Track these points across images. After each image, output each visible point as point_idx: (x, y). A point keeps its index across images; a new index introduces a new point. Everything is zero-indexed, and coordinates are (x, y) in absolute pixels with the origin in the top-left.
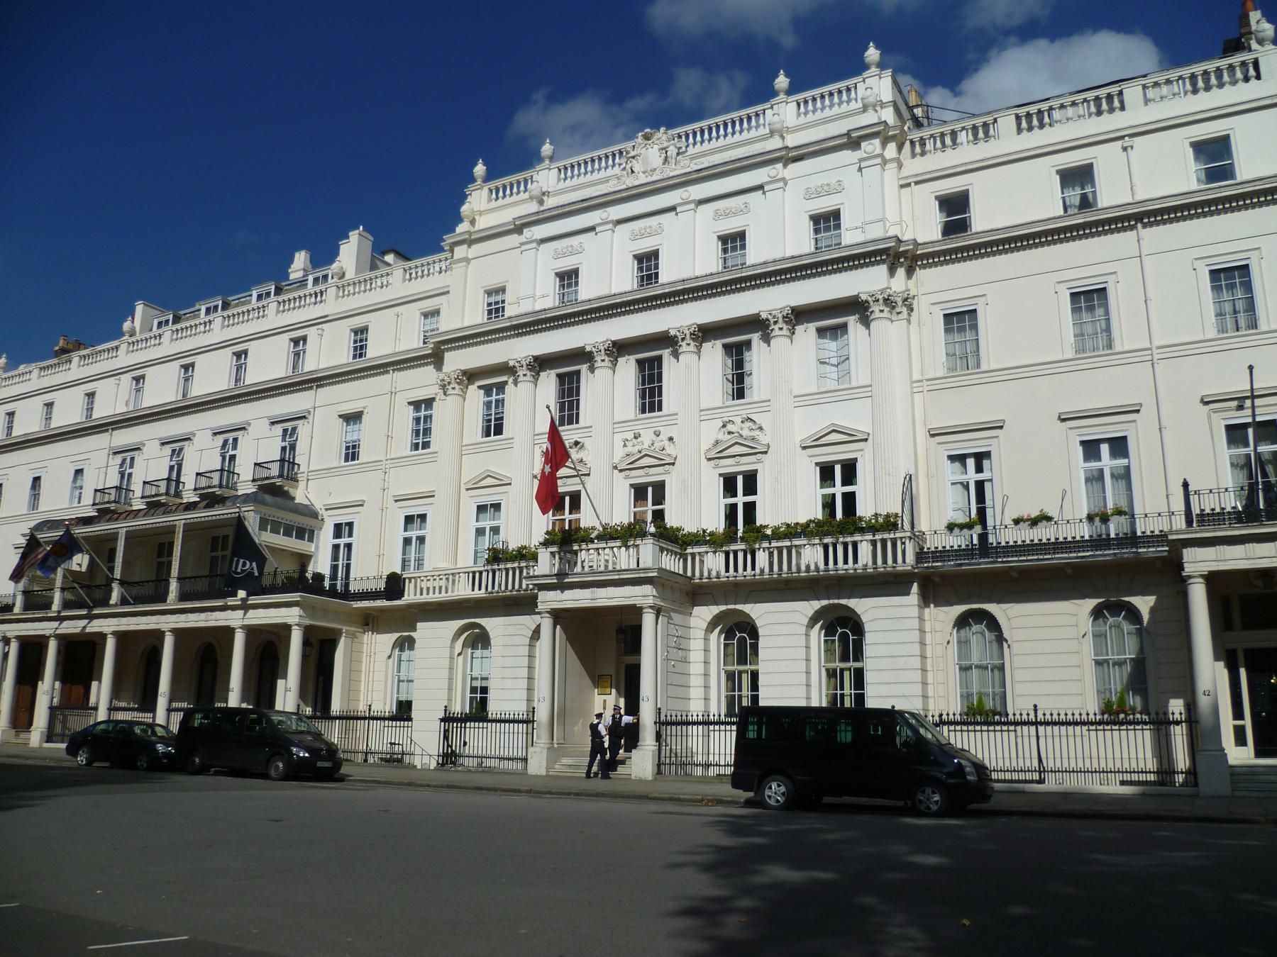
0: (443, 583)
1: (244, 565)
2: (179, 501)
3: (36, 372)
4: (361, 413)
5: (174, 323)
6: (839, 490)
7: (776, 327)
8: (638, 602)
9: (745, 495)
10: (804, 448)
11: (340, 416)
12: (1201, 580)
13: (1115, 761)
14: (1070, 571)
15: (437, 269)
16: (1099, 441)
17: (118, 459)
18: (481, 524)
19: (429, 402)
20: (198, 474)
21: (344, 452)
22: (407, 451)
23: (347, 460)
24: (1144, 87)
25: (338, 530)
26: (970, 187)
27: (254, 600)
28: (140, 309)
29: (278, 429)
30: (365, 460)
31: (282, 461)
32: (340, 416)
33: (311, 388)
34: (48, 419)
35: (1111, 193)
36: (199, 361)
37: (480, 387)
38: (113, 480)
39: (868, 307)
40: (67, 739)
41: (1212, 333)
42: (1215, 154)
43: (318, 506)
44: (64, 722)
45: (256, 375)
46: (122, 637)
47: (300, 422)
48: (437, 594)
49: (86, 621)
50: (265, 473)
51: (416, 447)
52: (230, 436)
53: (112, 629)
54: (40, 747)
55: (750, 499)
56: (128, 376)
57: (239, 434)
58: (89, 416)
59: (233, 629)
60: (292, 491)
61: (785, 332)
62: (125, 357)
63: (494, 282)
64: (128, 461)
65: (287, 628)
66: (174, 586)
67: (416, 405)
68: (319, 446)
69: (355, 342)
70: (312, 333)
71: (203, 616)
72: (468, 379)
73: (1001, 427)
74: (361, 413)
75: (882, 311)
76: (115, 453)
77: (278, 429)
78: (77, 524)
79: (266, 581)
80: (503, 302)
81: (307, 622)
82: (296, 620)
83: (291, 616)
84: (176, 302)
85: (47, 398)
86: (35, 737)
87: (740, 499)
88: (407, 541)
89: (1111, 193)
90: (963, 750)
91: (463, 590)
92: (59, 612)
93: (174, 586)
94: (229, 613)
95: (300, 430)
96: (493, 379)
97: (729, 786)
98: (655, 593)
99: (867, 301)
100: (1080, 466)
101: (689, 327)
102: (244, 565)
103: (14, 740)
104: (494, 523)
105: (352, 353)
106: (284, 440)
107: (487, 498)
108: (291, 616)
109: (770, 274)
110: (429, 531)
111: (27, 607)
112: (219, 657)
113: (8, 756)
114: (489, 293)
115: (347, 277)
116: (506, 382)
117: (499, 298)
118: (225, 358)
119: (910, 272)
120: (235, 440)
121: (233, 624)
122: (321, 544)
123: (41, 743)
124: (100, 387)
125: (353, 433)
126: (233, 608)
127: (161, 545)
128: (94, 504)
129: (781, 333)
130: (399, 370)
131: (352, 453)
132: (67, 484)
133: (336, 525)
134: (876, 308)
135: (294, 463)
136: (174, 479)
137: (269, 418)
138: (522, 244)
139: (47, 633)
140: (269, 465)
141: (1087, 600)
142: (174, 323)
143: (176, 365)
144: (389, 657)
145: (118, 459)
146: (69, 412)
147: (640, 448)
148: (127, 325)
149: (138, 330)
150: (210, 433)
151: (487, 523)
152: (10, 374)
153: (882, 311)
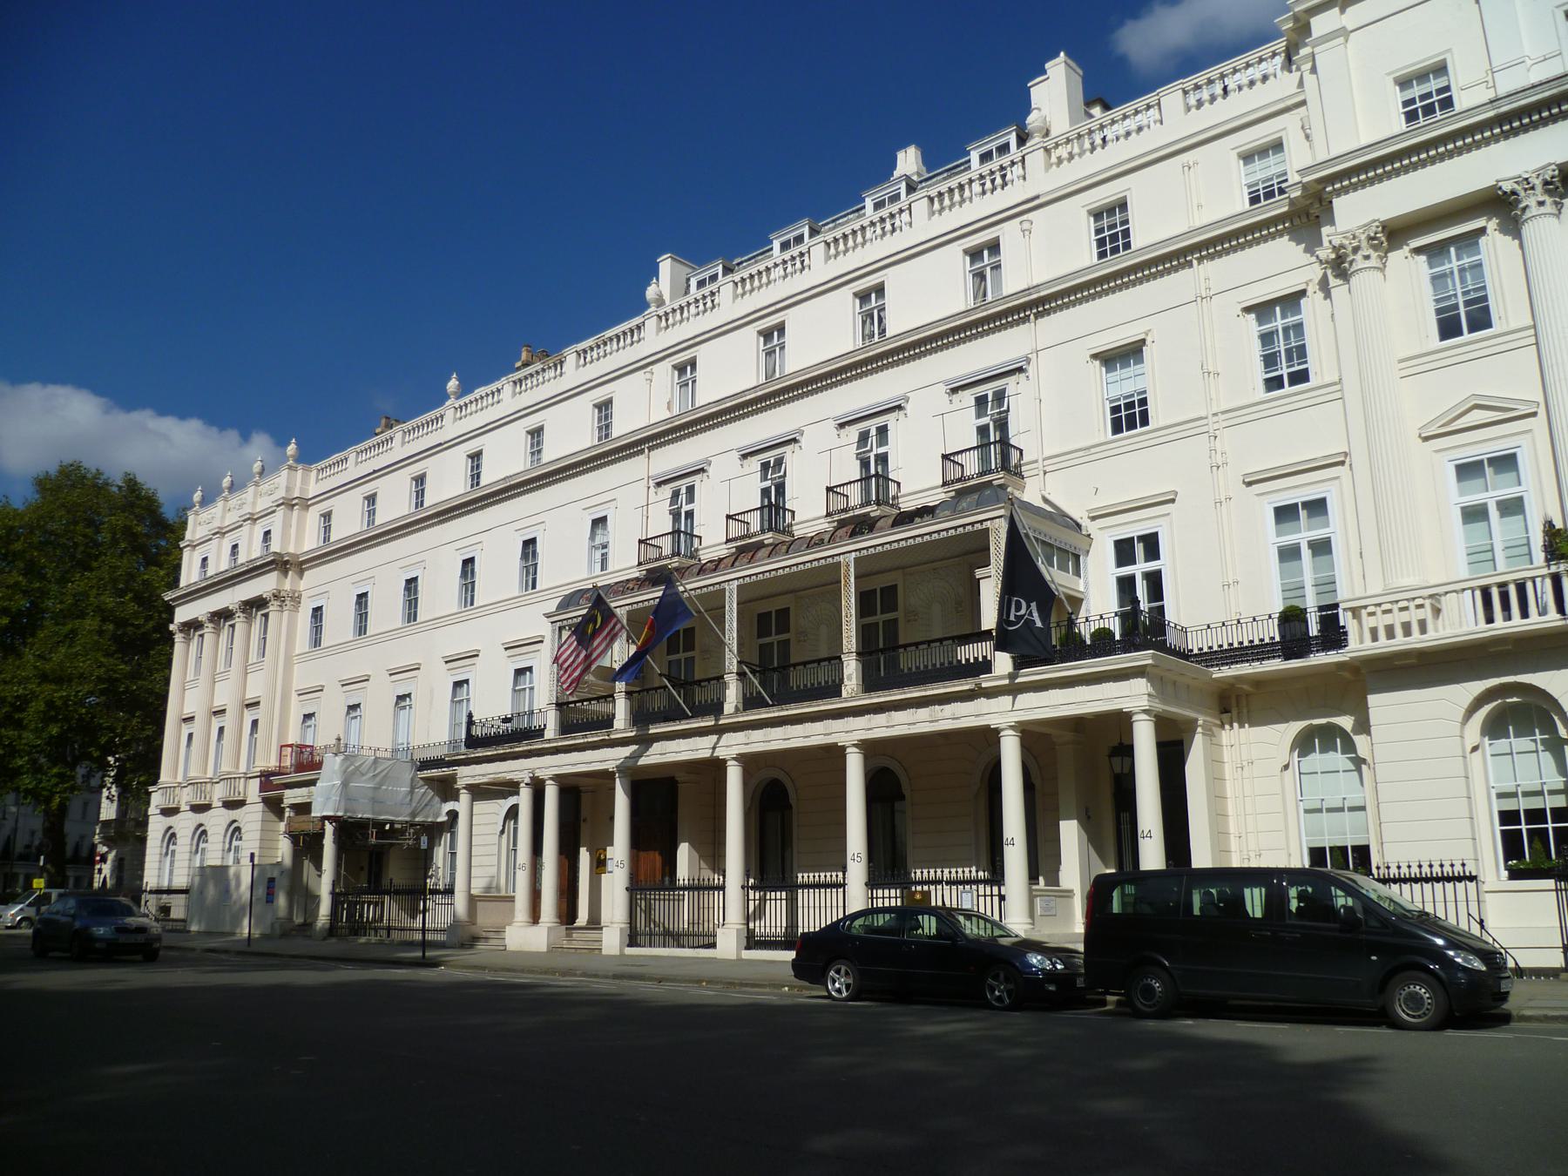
0: (1426, 613)
2: (693, 562)
3: (508, 389)
4: (1143, 341)
7: (1359, 257)
8: (1126, 705)
10: (1426, 439)
11: (1095, 356)
12: (1011, 732)
13: (527, 937)
14: (1346, 675)
15: (1087, 145)
17: (667, 491)
18: (1289, 539)
19: (1292, 301)
20: (729, 517)
21: (1109, 417)
22: (1260, 393)
23: (1117, 428)
24: (1185, 92)
25: (1124, 552)
26: (1282, 134)
27: (1029, 675)
28: (666, 265)
29: (755, 464)
30: (1162, 424)
31: (676, 532)
32: (1095, 356)
33: (642, 452)
34: (372, 513)
35: (1150, 230)
36: (702, 353)
37: (1418, 251)
38: (662, 523)
39: (1518, 201)
41: (1110, 437)
42: (1112, 228)
43: (1077, 512)
44: (648, 911)
45: (799, 357)
46: (1034, 737)
47: (788, 449)
48: (1368, 643)
49: (715, 737)
50: (653, 553)
51: (1274, 384)
52: (683, 485)
53: (735, 751)
54: (622, 955)
56: (667, 365)
57: (889, 419)
59: (997, 732)
61: (1374, 262)
62: (653, 338)
63: (1417, 56)
64: (683, 491)
65: (1120, 722)
66: (851, 668)
67: (1262, 310)
68: (1056, 411)
69: (1099, 231)
71: (923, 713)
72: (1388, 239)
73: (1173, 501)
74: (1143, 341)
75: (1541, 204)
76: (659, 484)
77: (755, 464)
78: (616, 593)
80: (1447, 88)
81: (1159, 707)
82: (1144, 703)
83: (1133, 696)
84: (728, 235)
85: (532, 422)
86: (611, 940)
88: (1289, 554)
89: (1150, 230)
90: (1423, 913)
91: (1462, 622)
92: (1012, 676)
94: (982, 704)
95: (788, 459)
98: (1150, 689)
99: (1514, 193)
100: (1271, 537)
101: (1538, 172)
103: (565, 944)
104: (1318, 534)
105: (1095, 251)
106: (764, 478)
107: (1297, 492)
108: (1133, 696)
110: (1336, 527)
111: (566, 728)
112: (793, 801)
113: (565, 973)
114: (1404, 83)
115: (1053, 133)
116: (1482, 231)
117: (1434, 84)
118: (843, 304)
119: (301, 573)
120: (691, 490)
121: (993, 721)
122: (1090, 579)
123: (621, 950)
124: (618, 391)
125: (1125, 383)
126: (991, 693)
129: (1367, 264)
130: (1211, 257)
131: (1129, 416)
132: (603, 532)
134: (1530, 201)
135: (692, 536)
136: (774, 506)
137: (946, 383)
139: (610, 766)
140: (845, 490)
141: (1285, 719)
143: (750, 332)
144: (502, 832)
145: (667, 491)
146: (570, 432)
148: (651, 292)
149: (666, 297)
150: (736, 455)
151: (1304, 533)
152: (466, 399)
153: (1541, 204)
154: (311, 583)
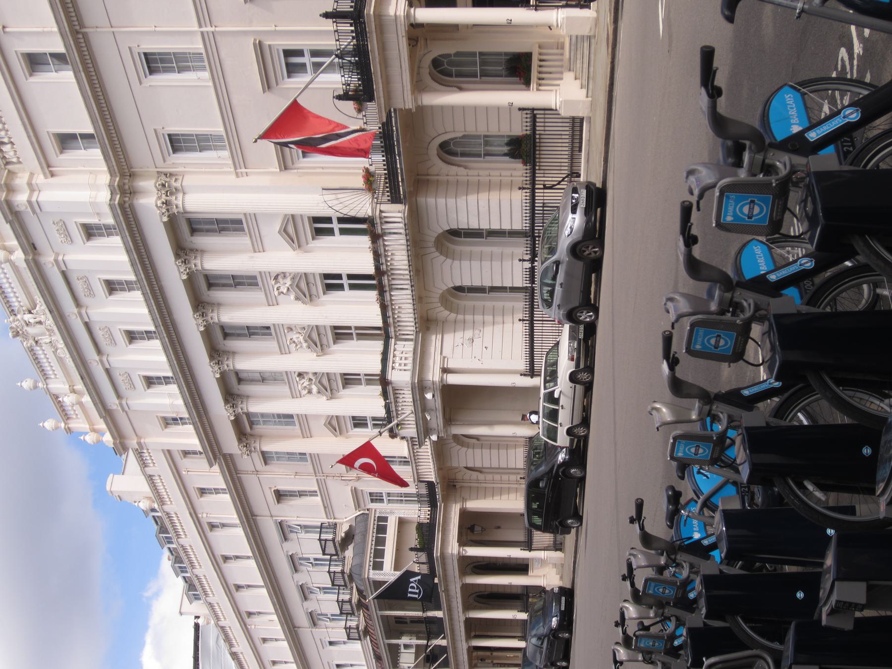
1: (413, 587)
5: (196, 590)
6: (307, 59)
9: (332, 223)
16: (287, 64)
40: (564, 321)
53: (461, 614)
55: (335, 221)
58: (59, 58)
59: (469, 647)
60: (345, 528)
66: (431, 614)
70: (204, 522)
79: (425, 569)
87: (336, 226)
93: (431, 614)
96: (244, 429)
97: (567, 536)
102: (413, 587)
109: (259, 550)
127: (397, 622)
128: (360, 639)
133: (372, 501)
138: (123, 410)
142: (196, 590)
147: (302, 341)
154: (145, 151)
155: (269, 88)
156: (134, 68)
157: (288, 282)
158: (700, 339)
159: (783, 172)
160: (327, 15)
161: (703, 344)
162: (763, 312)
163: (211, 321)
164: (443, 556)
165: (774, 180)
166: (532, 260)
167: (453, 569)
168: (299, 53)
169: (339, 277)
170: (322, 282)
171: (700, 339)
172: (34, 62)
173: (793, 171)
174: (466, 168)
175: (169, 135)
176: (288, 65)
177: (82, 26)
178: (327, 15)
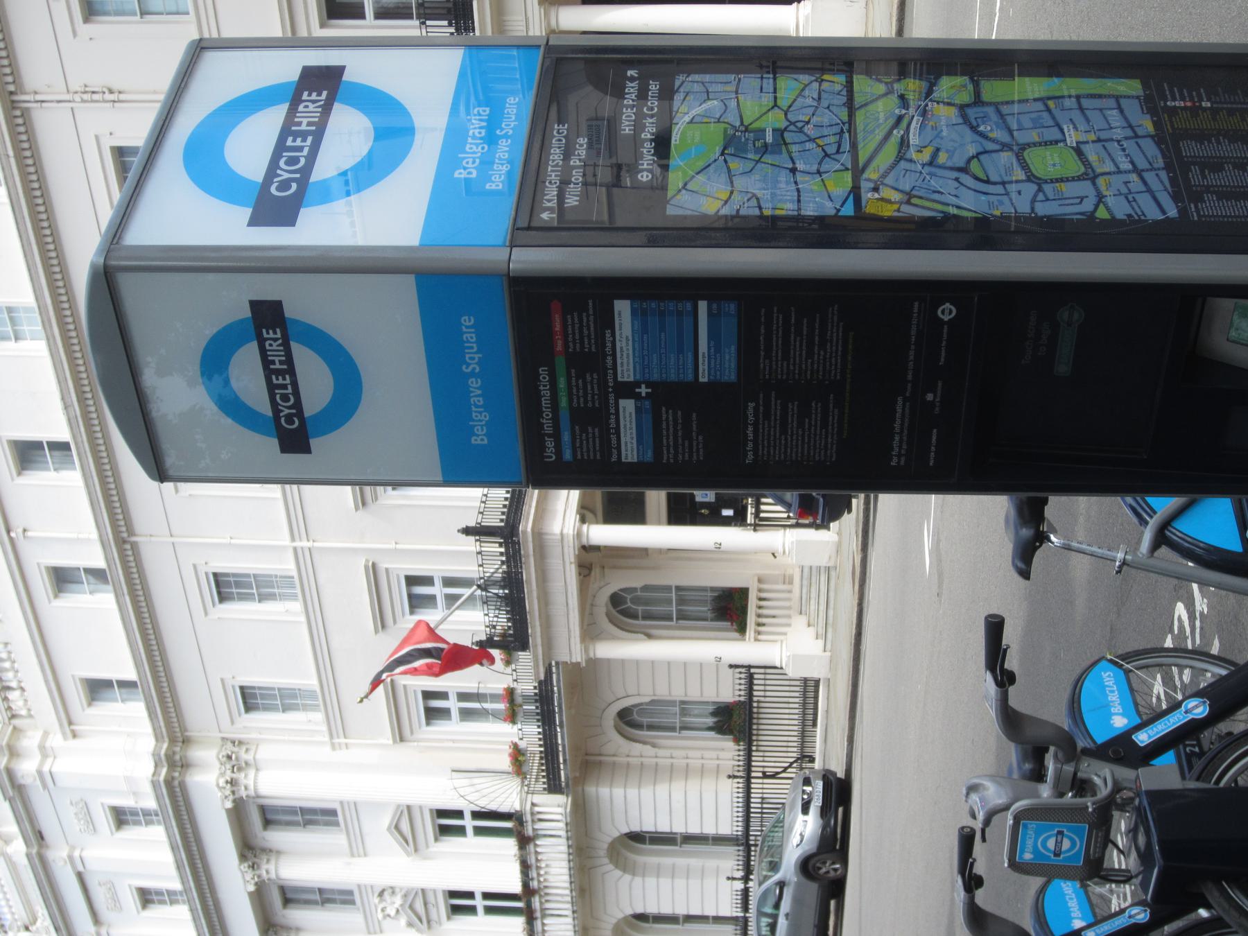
55: (467, 815)
154: (206, 708)
155: (383, 627)
156: (200, 593)
157: (398, 901)
158: (1030, 843)
159: (1103, 792)
160: (467, 531)
161: (1035, 851)
162: (1126, 794)
163: (243, 793)
164: (539, 536)
165: (1089, 803)
166: (746, 879)
167: (565, 579)
168: (428, 581)
169: (470, 895)
170: (433, 821)
171: (1030, 843)
172: (62, 578)
173: (1118, 788)
174: (654, 746)
175: (242, 688)
176: (411, 597)
177: (131, 532)
178: (467, 531)
